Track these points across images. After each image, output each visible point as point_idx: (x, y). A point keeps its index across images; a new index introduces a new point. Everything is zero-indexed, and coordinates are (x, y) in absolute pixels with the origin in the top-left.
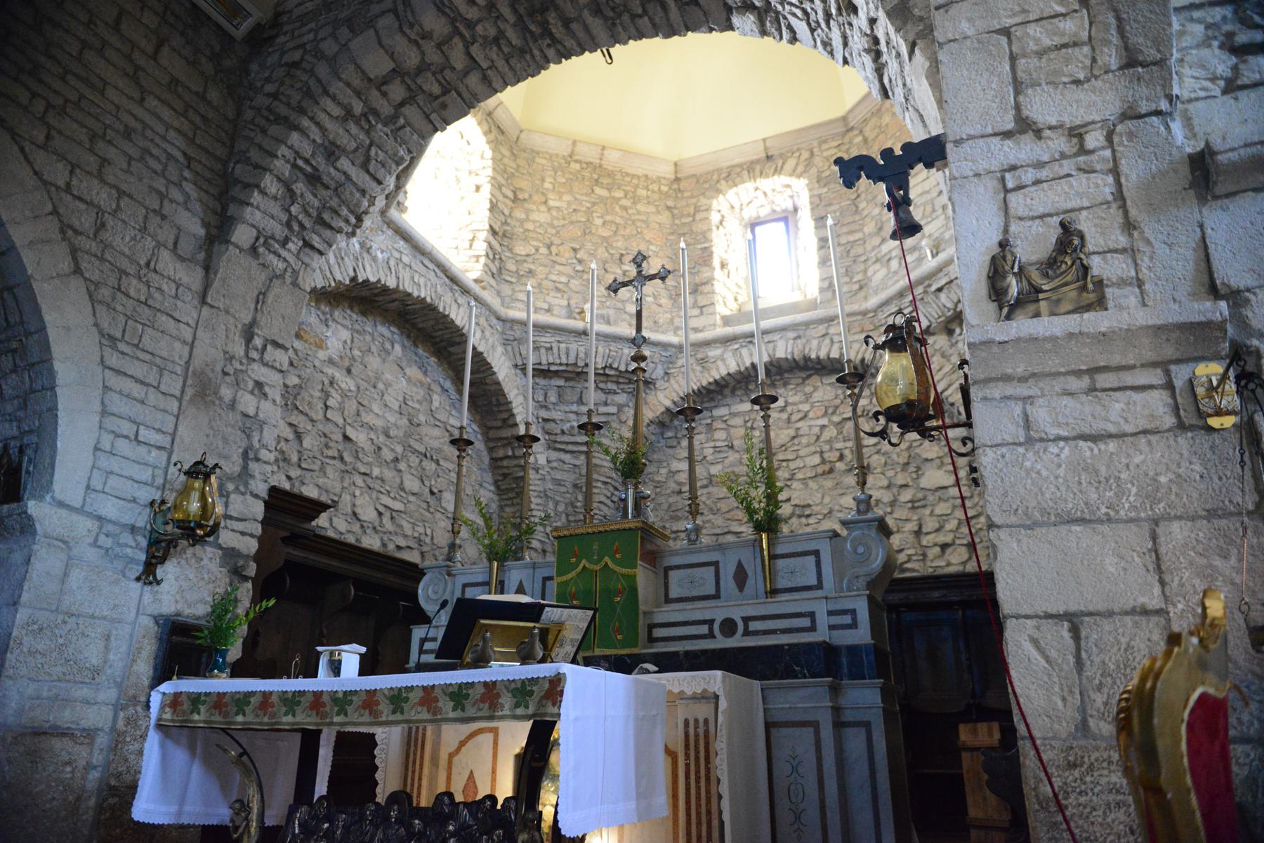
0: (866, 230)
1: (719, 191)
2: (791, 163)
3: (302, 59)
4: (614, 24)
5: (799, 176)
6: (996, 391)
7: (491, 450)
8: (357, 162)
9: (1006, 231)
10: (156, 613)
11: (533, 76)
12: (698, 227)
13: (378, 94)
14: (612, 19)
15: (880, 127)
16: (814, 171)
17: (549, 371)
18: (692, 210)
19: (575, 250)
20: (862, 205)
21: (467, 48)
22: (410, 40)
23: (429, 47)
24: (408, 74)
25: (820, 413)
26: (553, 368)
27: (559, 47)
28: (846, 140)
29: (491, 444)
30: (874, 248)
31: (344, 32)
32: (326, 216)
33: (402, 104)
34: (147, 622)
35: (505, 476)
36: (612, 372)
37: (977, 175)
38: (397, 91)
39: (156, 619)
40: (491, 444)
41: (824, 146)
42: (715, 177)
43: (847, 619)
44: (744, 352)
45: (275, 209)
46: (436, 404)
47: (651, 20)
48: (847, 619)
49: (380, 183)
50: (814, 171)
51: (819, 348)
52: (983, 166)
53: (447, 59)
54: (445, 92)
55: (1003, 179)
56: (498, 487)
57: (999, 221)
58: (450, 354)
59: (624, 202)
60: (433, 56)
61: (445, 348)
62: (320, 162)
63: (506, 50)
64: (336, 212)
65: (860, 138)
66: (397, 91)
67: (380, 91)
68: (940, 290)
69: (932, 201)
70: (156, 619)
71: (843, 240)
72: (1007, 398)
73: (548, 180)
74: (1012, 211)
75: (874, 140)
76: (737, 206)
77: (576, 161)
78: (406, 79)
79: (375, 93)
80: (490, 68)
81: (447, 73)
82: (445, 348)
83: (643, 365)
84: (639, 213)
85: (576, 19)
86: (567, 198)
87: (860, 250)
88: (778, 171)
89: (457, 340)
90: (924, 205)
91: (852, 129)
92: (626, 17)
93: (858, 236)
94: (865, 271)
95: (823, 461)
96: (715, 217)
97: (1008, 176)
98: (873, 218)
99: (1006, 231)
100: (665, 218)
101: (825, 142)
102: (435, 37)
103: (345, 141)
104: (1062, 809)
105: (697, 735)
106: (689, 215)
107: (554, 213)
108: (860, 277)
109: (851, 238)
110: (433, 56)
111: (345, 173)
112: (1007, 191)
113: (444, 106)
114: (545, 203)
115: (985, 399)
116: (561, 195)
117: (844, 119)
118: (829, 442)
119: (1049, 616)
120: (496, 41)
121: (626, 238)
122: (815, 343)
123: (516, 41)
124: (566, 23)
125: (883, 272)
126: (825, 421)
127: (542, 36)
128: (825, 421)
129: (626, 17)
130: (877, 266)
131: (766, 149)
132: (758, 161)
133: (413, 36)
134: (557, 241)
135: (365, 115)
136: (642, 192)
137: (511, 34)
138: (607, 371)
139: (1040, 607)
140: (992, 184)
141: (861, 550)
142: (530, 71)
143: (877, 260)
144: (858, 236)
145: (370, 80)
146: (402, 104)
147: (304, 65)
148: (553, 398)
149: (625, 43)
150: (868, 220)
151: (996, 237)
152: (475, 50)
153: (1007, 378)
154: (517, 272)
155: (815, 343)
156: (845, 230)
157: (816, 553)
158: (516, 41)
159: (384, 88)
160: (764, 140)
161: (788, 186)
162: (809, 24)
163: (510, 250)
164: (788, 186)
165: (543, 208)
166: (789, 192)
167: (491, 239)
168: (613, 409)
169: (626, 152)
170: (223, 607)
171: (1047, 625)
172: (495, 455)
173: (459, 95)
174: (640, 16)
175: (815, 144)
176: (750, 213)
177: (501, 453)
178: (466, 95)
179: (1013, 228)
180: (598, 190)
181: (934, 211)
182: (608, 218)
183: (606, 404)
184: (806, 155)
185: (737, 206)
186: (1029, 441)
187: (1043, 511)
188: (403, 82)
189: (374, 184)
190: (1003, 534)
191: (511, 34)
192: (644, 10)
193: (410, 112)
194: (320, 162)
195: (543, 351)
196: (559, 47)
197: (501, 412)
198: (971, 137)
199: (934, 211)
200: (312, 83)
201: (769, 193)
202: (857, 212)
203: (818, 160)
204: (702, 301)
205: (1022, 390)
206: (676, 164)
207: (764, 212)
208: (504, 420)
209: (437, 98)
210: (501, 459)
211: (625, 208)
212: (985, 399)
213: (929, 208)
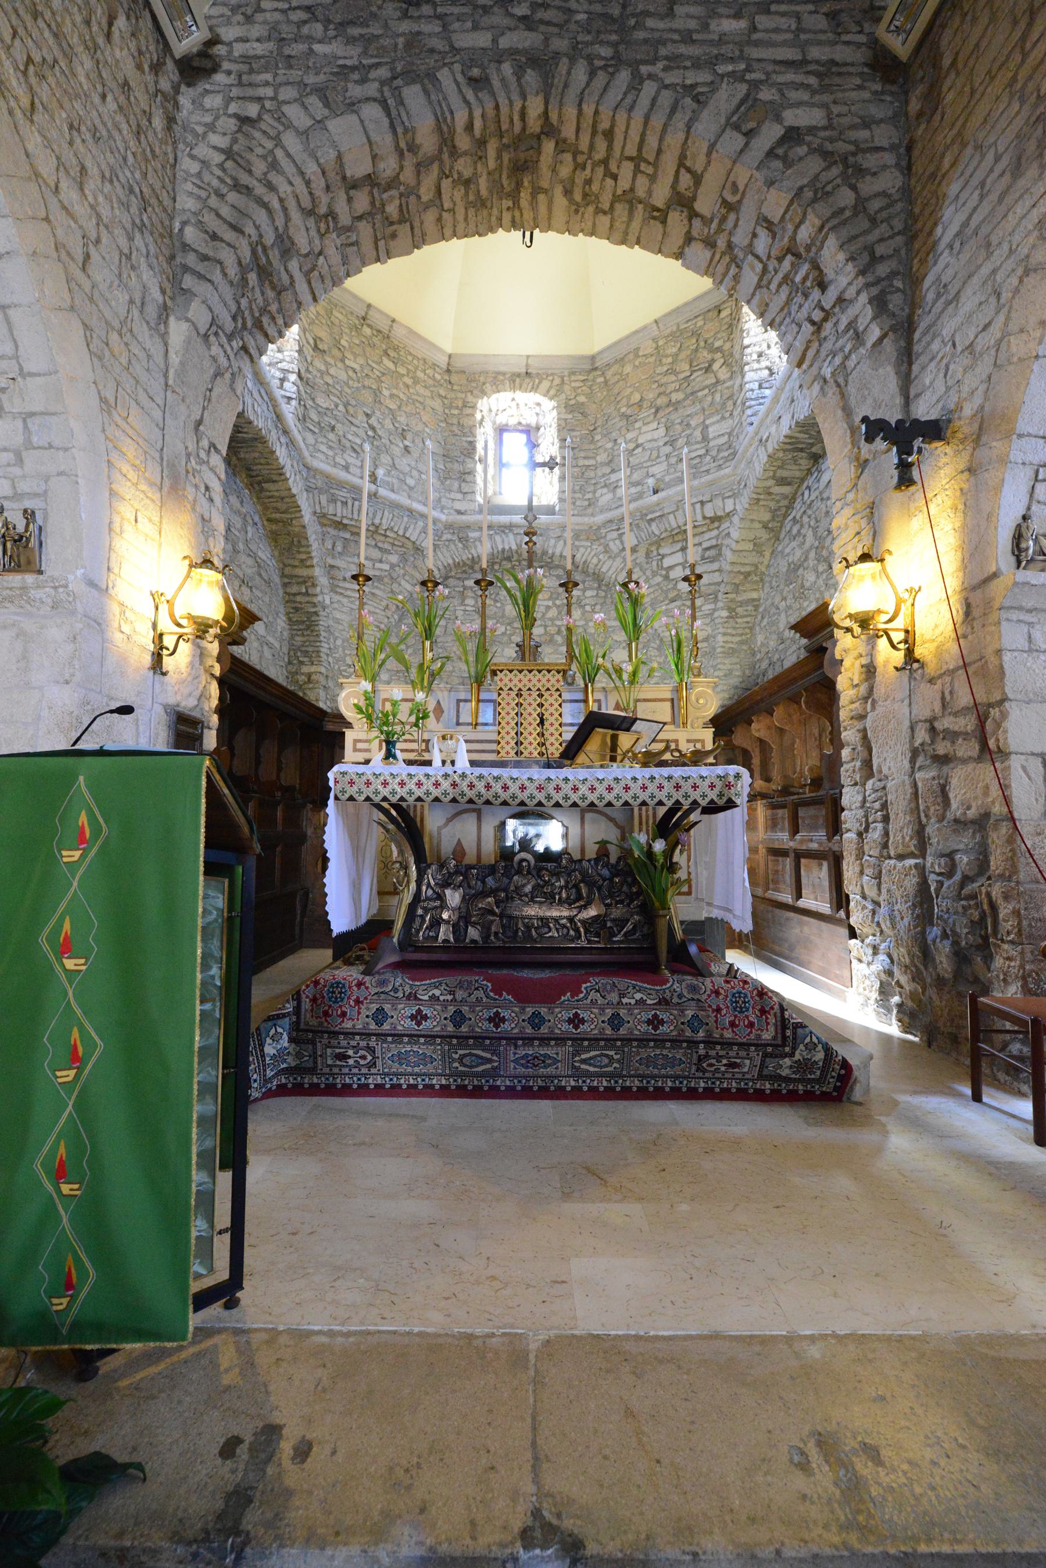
0: (598, 458)
1: (484, 393)
2: (546, 384)
3: (260, 118)
4: (577, 211)
5: (551, 399)
6: (1015, 615)
7: (285, 585)
8: (305, 269)
9: (1029, 509)
10: (164, 702)
11: (480, 235)
12: (465, 421)
13: (345, 197)
14: (578, 204)
15: (621, 374)
16: (563, 396)
17: (341, 523)
18: (460, 404)
19: (367, 415)
20: (598, 437)
21: (440, 179)
22: (397, 146)
23: (409, 161)
24: (378, 185)
25: (547, 596)
26: (345, 521)
27: (517, 214)
28: (591, 377)
29: (286, 580)
30: (604, 475)
31: (318, 108)
32: (265, 320)
33: (360, 218)
34: (159, 710)
35: (297, 609)
36: (392, 535)
37: (1024, 464)
38: (362, 201)
39: (166, 707)
40: (286, 580)
41: (573, 378)
42: (482, 379)
43: (360, 746)
44: (498, 538)
45: (228, 292)
46: (250, 535)
47: (612, 220)
48: (360, 746)
49: (315, 300)
50: (563, 396)
51: (555, 546)
52: (1029, 458)
53: (419, 184)
54: (402, 221)
55: (1037, 472)
56: (290, 619)
57: (1025, 500)
58: (262, 490)
59: (406, 380)
60: (408, 176)
61: (259, 483)
62: (275, 255)
63: (471, 198)
64: (273, 319)
65: (602, 379)
66: (362, 201)
67: (347, 194)
68: (652, 520)
69: (658, 448)
70: (166, 707)
71: (581, 462)
72: (1020, 621)
73: (345, 337)
74: (1036, 496)
75: (614, 384)
76: (494, 410)
77: (369, 326)
78: (375, 191)
79: (342, 196)
80: (449, 210)
81: (413, 199)
82: (259, 483)
83: (534, 538)
84: (418, 394)
85: (546, 191)
86: (361, 360)
87: (592, 474)
88: (534, 389)
89: (275, 478)
90: (651, 450)
91: (596, 369)
92: (591, 209)
93: (592, 462)
94: (595, 492)
95: (546, 633)
96: (478, 416)
97: (1041, 470)
98: (606, 450)
99: (1029, 509)
100: (437, 404)
101: (574, 373)
102: (421, 154)
103: (302, 242)
104: (1032, 856)
105: (647, 816)
106: (457, 408)
107: (351, 373)
108: (589, 496)
109: (587, 462)
110: (408, 176)
111: (291, 277)
112: (1036, 480)
113: (394, 236)
114: (342, 361)
115: (1008, 620)
116: (355, 355)
117: (593, 358)
118: (552, 620)
119: (1033, 754)
120: (467, 183)
121: (408, 415)
122: (552, 541)
123: (484, 192)
124: (536, 191)
125: (610, 496)
126: (550, 603)
127: (509, 195)
128: (550, 603)
129: (591, 209)
130: (605, 490)
131: (527, 365)
132: (519, 375)
133: (403, 145)
134: (353, 403)
135: (326, 216)
136: (420, 374)
137: (483, 183)
138: (388, 533)
139: (1029, 748)
140: (1030, 472)
141: (701, 701)
142: (481, 229)
143: (606, 486)
144: (592, 462)
145: (344, 178)
146: (360, 218)
147: (263, 126)
148: (339, 549)
149: (576, 235)
150: (601, 450)
151: (1022, 511)
152: (446, 184)
153: (1020, 608)
154: (319, 423)
155: (552, 541)
156: (582, 454)
157: (459, 701)
158: (484, 192)
159: (352, 192)
160: (528, 357)
161: (538, 404)
162: (761, 279)
163: (313, 400)
164: (538, 404)
165: (340, 365)
166: (538, 409)
167: (299, 382)
168: (386, 567)
169: (411, 332)
170: (203, 696)
171: (1031, 759)
172: (289, 590)
173: (412, 228)
174: (605, 213)
175: (566, 373)
176: (501, 419)
177: (294, 589)
178: (417, 231)
179: (1034, 508)
180: (386, 361)
181: (658, 457)
182: (395, 391)
183: (381, 561)
184: (557, 381)
185: (494, 410)
186: (1030, 651)
187: (1035, 694)
188: (371, 193)
189: (309, 298)
190: (1013, 704)
191: (483, 183)
192: (612, 207)
193: (365, 229)
194: (275, 255)
195: (339, 504)
196: (517, 214)
197: (299, 552)
198: (1029, 435)
199: (658, 457)
200: (279, 153)
201: (522, 406)
202: (592, 442)
203: (566, 388)
204: (465, 488)
205: (1028, 618)
206: (450, 356)
207: (512, 422)
208: (302, 561)
209: (392, 224)
210: (295, 595)
211: (407, 386)
212: (1008, 620)
213: (655, 454)
